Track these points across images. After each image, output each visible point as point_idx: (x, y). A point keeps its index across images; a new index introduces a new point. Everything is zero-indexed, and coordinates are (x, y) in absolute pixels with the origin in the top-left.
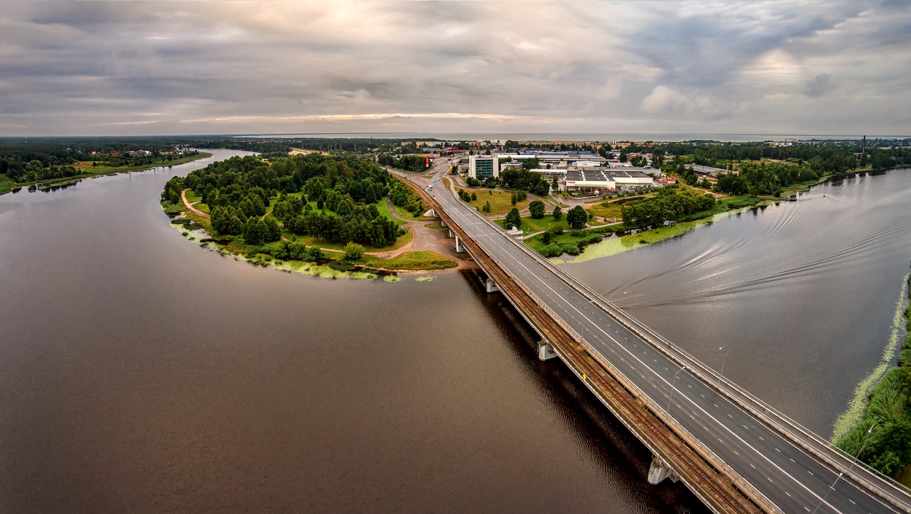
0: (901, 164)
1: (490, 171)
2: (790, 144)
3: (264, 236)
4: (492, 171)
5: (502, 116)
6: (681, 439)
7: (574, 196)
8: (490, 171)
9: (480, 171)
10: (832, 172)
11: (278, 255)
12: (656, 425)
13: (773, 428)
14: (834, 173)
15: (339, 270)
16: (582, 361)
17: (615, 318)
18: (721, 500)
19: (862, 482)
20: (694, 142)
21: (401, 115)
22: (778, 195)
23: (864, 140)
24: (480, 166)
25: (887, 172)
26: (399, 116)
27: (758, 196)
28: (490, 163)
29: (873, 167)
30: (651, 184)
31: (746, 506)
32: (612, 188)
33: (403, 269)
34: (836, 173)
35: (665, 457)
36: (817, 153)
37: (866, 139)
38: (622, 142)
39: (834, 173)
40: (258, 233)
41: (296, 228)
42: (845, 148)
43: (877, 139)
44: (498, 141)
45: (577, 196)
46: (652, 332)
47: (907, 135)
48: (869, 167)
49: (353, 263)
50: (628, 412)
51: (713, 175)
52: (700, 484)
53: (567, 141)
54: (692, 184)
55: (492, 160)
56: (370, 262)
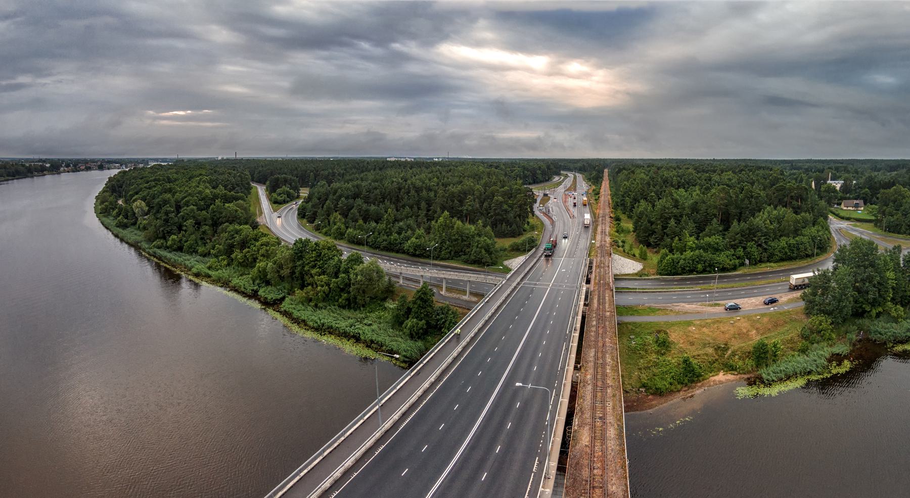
0: (4, 177)
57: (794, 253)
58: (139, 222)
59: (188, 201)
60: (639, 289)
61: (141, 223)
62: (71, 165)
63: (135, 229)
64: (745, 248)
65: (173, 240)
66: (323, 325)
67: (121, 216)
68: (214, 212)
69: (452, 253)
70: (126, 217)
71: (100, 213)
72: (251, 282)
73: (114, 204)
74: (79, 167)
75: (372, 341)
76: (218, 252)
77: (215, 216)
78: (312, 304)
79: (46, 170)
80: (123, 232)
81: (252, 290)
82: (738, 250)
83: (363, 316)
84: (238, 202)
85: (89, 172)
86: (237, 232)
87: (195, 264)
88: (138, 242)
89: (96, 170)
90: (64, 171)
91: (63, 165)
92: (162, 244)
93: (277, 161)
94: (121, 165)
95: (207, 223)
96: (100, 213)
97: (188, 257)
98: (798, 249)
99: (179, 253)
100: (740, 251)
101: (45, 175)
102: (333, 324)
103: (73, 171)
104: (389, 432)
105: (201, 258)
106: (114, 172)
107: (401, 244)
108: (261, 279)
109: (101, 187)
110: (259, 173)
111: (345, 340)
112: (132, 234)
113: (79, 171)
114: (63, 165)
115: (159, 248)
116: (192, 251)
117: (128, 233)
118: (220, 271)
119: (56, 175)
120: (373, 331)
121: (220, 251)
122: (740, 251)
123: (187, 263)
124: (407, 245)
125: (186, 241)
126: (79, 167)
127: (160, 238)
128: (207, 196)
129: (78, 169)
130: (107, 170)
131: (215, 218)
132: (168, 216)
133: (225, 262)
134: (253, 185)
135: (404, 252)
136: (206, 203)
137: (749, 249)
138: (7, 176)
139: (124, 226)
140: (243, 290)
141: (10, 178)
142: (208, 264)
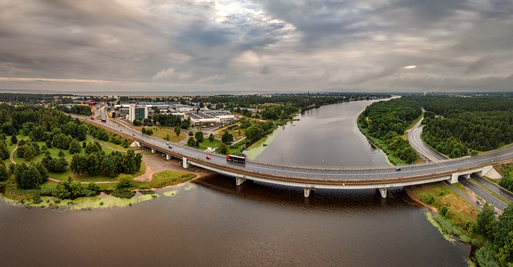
1: (143, 115)
2: (270, 96)
3: (38, 180)
4: (144, 115)
5: (102, 81)
7: (204, 128)
8: (143, 115)
9: (137, 116)
11: (63, 195)
14: (302, 108)
15: (125, 197)
20: (223, 95)
21: (43, 79)
22: (291, 118)
24: (137, 112)
25: (320, 107)
26: (41, 80)
27: (284, 120)
28: (143, 110)
29: (316, 105)
30: (233, 118)
32: (219, 122)
33: (168, 185)
36: (289, 100)
38: (188, 96)
40: (32, 177)
41: (57, 168)
43: (305, 93)
44: (113, 96)
45: (206, 128)
48: (314, 105)
49: (129, 190)
51: (254, 112)
53: (167, 96)
54: (250, 117)
55: (144, 108)
56: (142, 186)
59: (383, 122)
60: (265, 162)
62: (355, 97)
70: (365, 124)
79: (343, 100)
84: (399, 123)
85: (362, 101)
86: (391, 134)
90: (351, 101)
91: (351, 97)
93: (447, 96)
94: (377, 98)
99: (375, 138)
101: (342, 102)
103: (355, 101)
104: (268, 163)
106: (370, 102)
112: (366, 130)
113: (357, 100)
114: (351, 97)
115: (370, 136)
116: (378, 138)
119: (347, 102)
129: (357, 99)
139: (363, 127)
141: (328, 103)
142: (380, 142)
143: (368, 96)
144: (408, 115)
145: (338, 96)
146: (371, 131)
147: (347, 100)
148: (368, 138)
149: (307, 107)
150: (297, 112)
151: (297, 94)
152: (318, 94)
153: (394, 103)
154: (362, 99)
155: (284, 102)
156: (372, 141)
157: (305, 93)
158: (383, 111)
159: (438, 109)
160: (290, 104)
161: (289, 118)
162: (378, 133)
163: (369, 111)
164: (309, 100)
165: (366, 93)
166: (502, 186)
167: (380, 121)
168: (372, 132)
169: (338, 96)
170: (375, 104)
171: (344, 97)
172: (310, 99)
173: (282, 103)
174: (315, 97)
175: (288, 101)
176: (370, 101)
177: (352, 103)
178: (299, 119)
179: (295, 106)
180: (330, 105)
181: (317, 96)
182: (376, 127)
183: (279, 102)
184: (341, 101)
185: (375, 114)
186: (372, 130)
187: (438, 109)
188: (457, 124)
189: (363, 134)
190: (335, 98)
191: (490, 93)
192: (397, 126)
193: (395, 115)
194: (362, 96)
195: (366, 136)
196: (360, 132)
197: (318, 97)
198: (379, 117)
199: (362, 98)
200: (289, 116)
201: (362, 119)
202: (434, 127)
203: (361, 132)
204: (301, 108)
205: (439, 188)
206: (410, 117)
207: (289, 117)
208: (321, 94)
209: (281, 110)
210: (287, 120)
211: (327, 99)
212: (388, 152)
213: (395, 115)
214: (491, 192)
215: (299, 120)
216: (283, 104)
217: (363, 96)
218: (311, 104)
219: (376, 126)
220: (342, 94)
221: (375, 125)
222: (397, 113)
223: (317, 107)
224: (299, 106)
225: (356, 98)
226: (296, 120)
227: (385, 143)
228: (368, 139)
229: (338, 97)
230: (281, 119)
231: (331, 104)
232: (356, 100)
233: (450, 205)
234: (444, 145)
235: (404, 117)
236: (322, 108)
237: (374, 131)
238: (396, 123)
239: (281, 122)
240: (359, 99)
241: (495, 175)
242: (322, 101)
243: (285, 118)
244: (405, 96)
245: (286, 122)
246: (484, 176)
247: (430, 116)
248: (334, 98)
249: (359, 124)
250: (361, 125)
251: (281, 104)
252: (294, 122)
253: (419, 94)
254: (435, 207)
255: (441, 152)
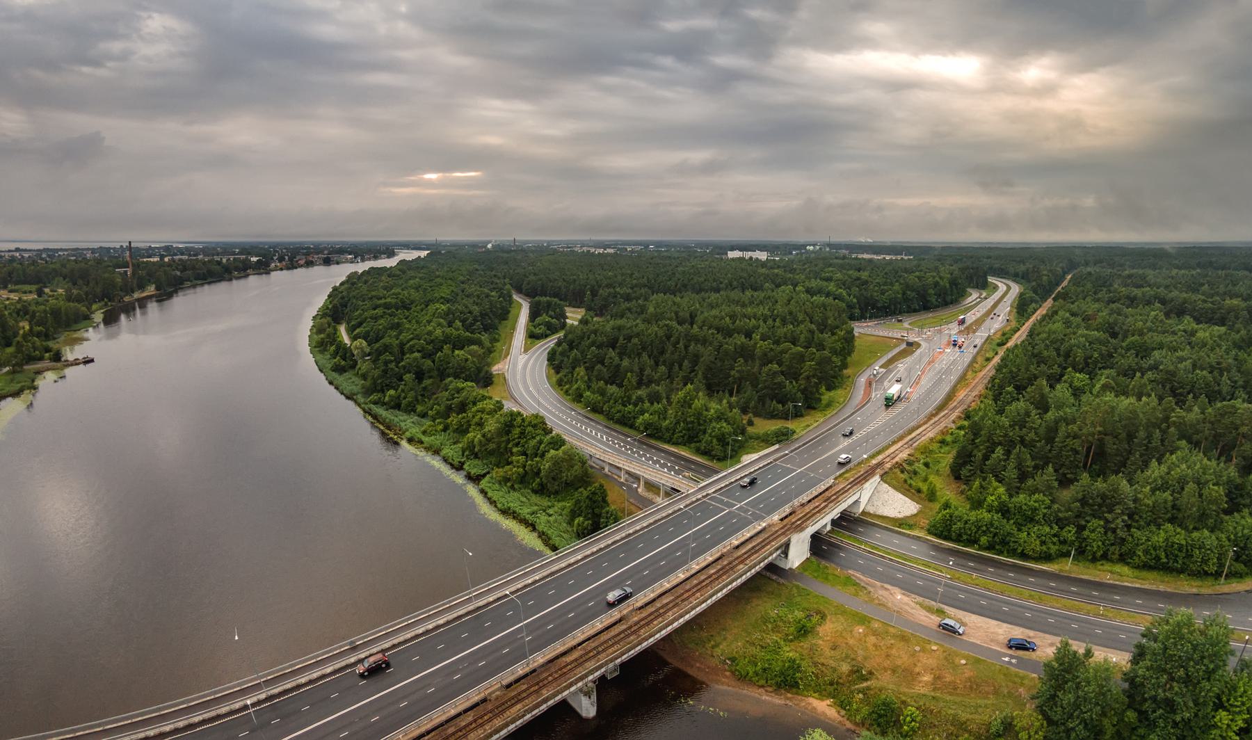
0: (191, 281)
6: (575, 647)
10: (103, 303)
12: (545, 675)
13: (400, 644)
16: (649, 619)
17: (219, 717)
18: (660, 619)
19: (572, 561)
22: (57, 357)
23: (130, 248)
27: (25, 367)
29: (157, 289)
31: (665, 601)
34: (109, 303)
35: (586, 676)
36: (56, 273)
37: (132, 245)
39: (106, 305)
42: (107, 259)
43: (122, 246)
46: (495, 582)
47: (187, 240)
48: (151, 290)
50: (519, 706)
52: (640, 636)
57: (1177, 562)
58: (358, 367)
59: (413, 346)
61: (360, 368)
62: (287, 257)
63: (354, 375)
64: (1081, 528)
65: (390, 396)
66: (509, 508)
67: (338, 358)
68: (441, 361)
69: (686, 438)
71: (315, 347)
72: (461, 453)
73: (332, 336)
74: (297, 261)
75: (543, 533)
76: (437, 414)
77: (442, 365)
78: (509, 484)
80: (340, 379)
81: (460, 462)
82: (1068, 528)
83: (550, 504)
86: (459, 391)
87: (411, 427)
88: (354, 394)
89: (320, 264)
90: (276, 269)
91: (275, 258)
92: (380, 398)
94: (355, 258)
95: (432, 374)
96: (315, 347)
97: (405, 417)
98: (1189, 556)
100: (1070, 532)
102: (517, 510)
103: (288, 269)
105: (419, 419)
106: (339, 273)
107: (634, 418)
108: (470, 451)
109: (320, 300)
110: (528, 284)
111: (522, 528)
113: (296, 268)
114: (275, 258)
115: (375, 403)
116: (410, 409)
117: (345, 380)
118: (433, 438)
120: (549, 522)
121: (438, 413)
122: (1070, 533)
123: (403, 424)
124: (640, 420)
125: (405, 398)
126: (297, 261)
127: (378, 391)
128: (437, 338)
129: (295, 264)
130: (336, 266)
131: (442, 368)
132: (387, 366)
133: (441, 427)
134: (516, 297)
135: (635, 429)
136: (433, 348)
137: (1086, 533)
138: (195, 279)
139: (339, 370)
140: (451, 461)
141: (199, 282)
143: (326, 252)
144: (486, 314)
145: (234, 254)
146: (375, 383)
147: (263, 267)
148: (370, 414)
149: (127, 299)
150: (86, 322)
151: (93, 251)
152: (168, 249)
153: (421, 275)
154: (309, 264)
155: (38, 283)
156: (389, 428)
157: (122, 246)
158: (396, 303)
159: (560, 288)
160: (58, 292)
161: (47, 355)
162: (403, 391)
163: (346, 306)
164: (134, 273)
165: (320, 244)
166: (939, 536)
167: (402, 345)
168: (379, 388)
169: (234, 254)
170: (353, 279)
171: (254, 259)
172: (137, 266)
173: (27, 287)
174: (156, 259)
175: (53, 278)
176: (334, 268)
177: (280, 277)
178: (91, 356)
179: (78, 300)
180: (206, 287)
181: (162, 257)
182: (392, 369)
183: (17, 283)
184: (245, 269)
185: (376, 318)
186: (379, 381)
187: (560, 288)
188: (668, 337)
189: (343, 397)
190: (224, 260)
191: (659, 244)
192: (467, 360)
193: (450, 318)
194: (307, 254)
195: (359, 405)
196: (332, 388)
197: (166, 259)
198: (391, 328)
199: (311, 259)
200: (51, 344)
201: (329, 336)
202: (597, 352)
203: (337, 388)
204: (103, 303)
205: (774, 601)
206: (490, 318)
207: (48, 350)
208: (177, 248)
209: (17, 322)
210: (39, 365)
211: (197, 266)
212: (474, 467)
213: (450, 318)
214: (941, 571)
215: (92, 361)
216: (30, 292)
217: (312, 253)
218: (142, 287)
219: (392, 365)
220: (248, 249)
221: (386, 363)
222: (449, 312)
223: (164, 296)
224: (90, 299)
225: (291, 259)
226: (76, 363)
227: (445, 430)
228: (367, 412)
229: (234, 259)
230: (14, 366)
231: (209, 283)
232: (292, 266)
233: (871, 673)
234: (663, 415)
235: (475, 320)
236: (182, 302)
237: (389, 387)
238: (462, 348)
239: (12, 380)
240: (302, 262)
241: (898, 505)
242: (178, 273)
243: (31, 359)
244: (440, 252)
245: (33, 381)
246: (864, 513)
247: (551, 313)
248: (219, 263)
249: (319, 357)
250: (325, 358)
251: (25, 292)
252: (69, 372)
253: (474, 245)
254: (816, 695)
255: (660, 438)
